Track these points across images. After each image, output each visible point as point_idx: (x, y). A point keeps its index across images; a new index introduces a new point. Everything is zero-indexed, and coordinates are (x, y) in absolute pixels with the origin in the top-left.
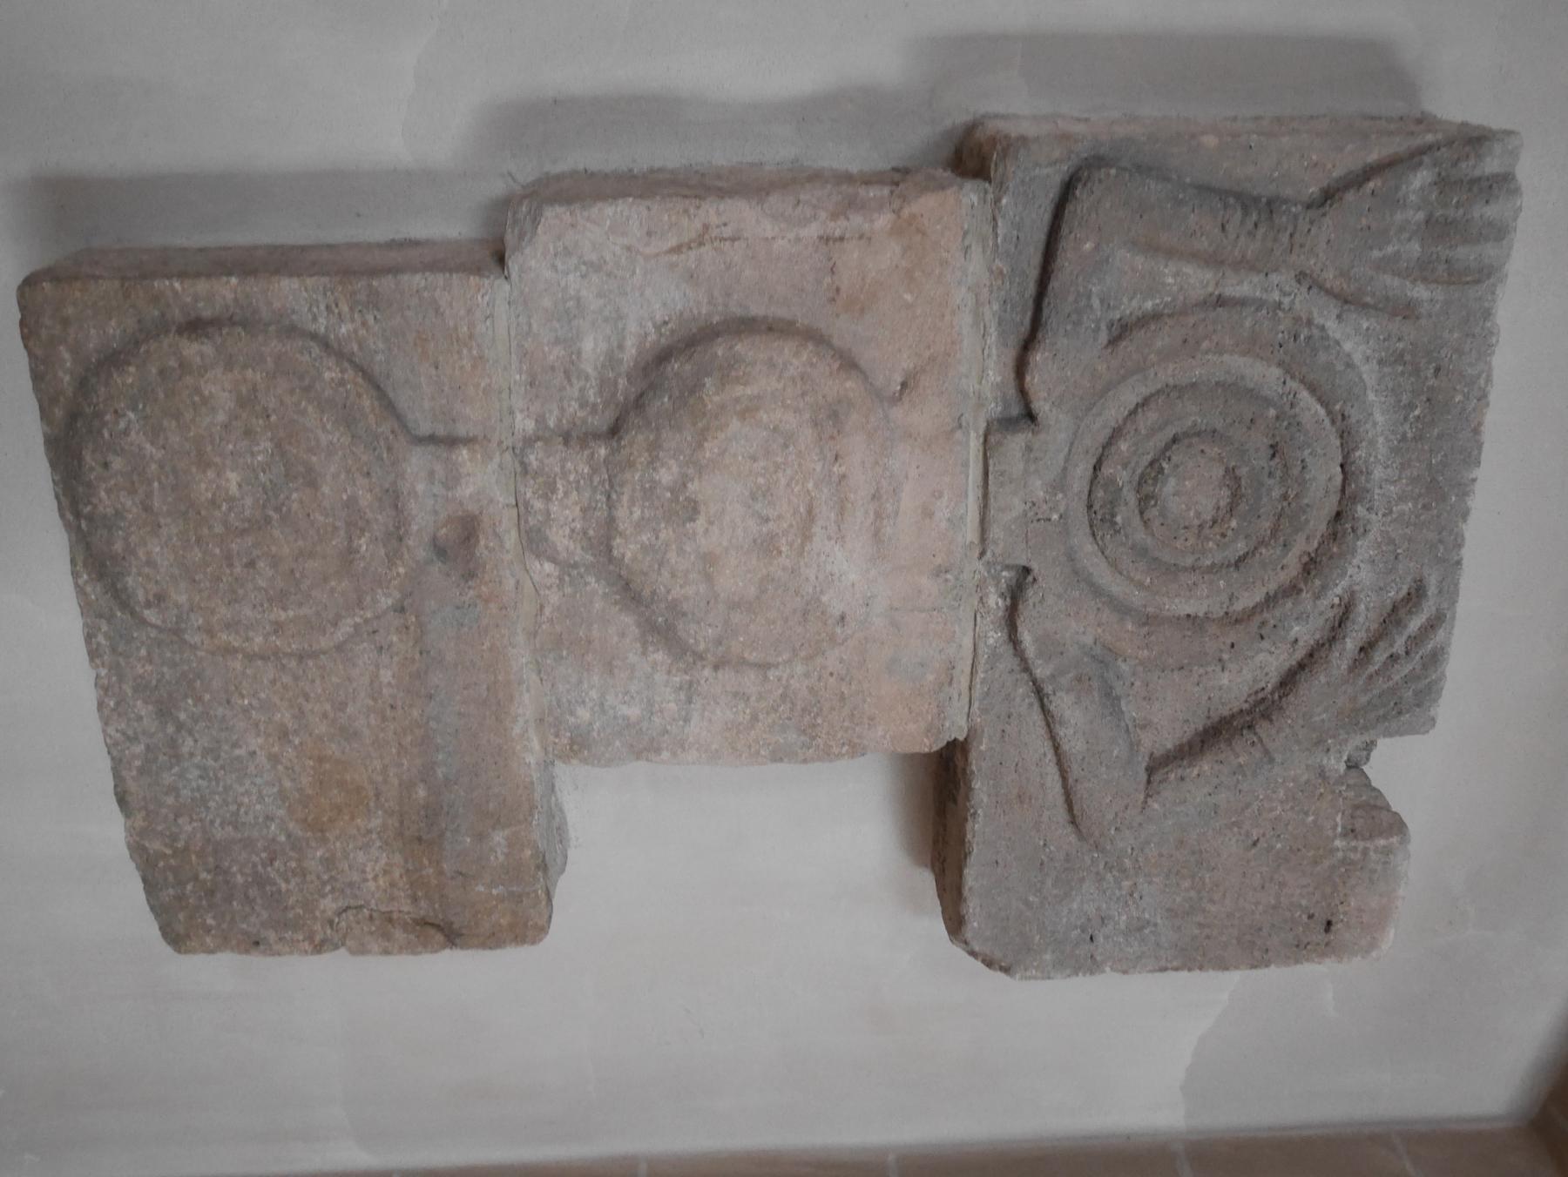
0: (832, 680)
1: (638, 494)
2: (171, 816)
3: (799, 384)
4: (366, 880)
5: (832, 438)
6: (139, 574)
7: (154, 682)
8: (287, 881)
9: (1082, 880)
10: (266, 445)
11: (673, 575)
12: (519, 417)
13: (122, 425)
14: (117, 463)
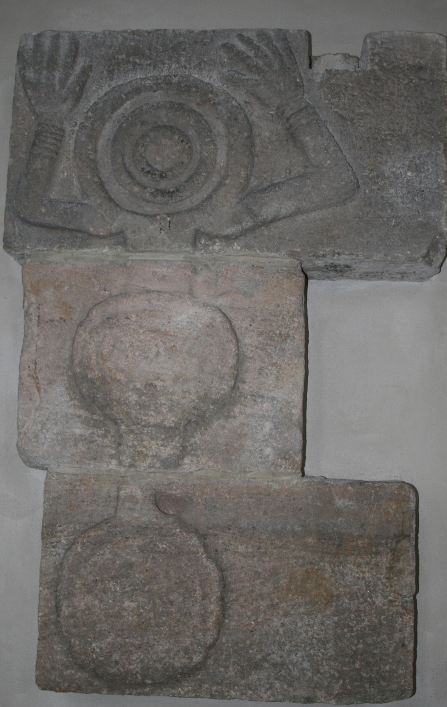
0: (254, 325)
1: (142, 412)
2: (319, 675)
3: (92, 335)
4: (364, 578)
5: (118, 320)
6: (174, 659)
7: (239, 668)
8: (364, 620)
9: (382, 197)
10: (111, 585)
11: (184, 398)
12: (111, 467)
13: (98, 650)
14: (116, 657)
